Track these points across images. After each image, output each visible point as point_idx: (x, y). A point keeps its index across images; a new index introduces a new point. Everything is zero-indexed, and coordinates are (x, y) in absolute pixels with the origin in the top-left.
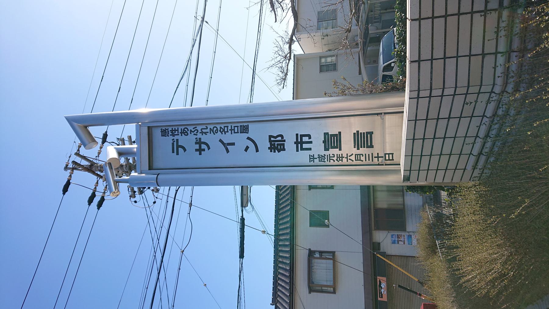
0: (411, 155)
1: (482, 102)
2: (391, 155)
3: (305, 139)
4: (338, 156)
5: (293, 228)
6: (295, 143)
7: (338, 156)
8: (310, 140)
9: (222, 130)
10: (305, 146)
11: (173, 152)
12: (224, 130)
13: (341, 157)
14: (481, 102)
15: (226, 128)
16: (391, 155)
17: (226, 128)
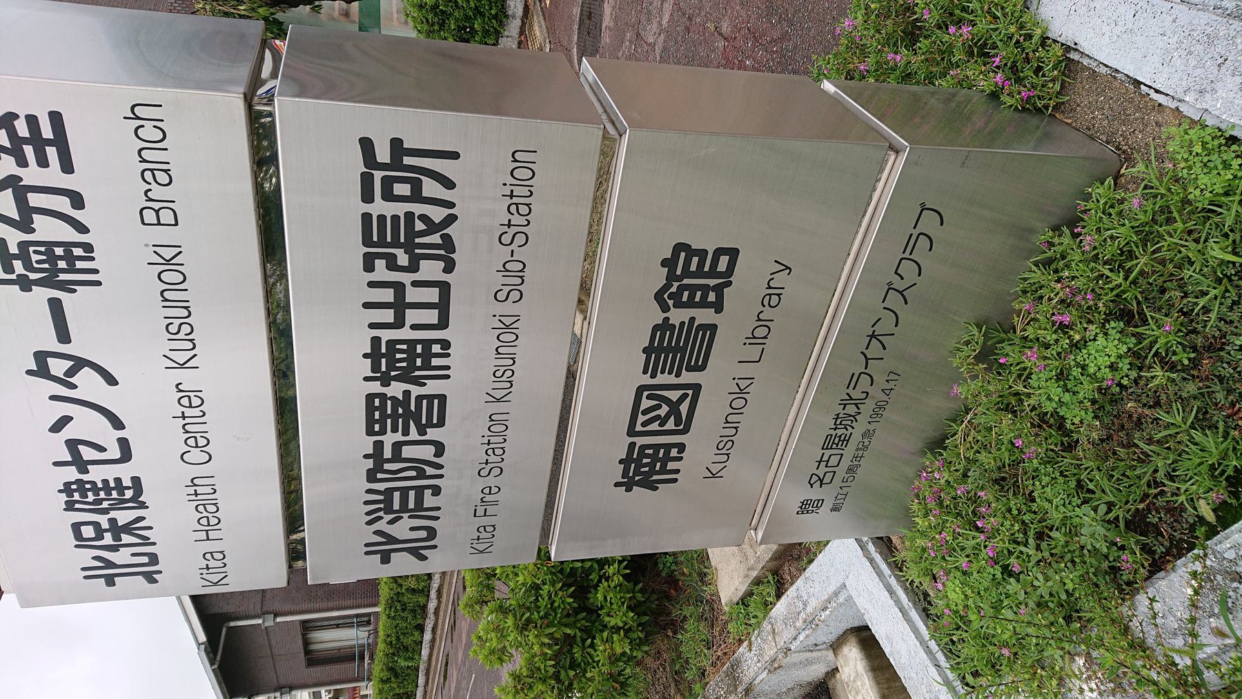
10: (388, 295)
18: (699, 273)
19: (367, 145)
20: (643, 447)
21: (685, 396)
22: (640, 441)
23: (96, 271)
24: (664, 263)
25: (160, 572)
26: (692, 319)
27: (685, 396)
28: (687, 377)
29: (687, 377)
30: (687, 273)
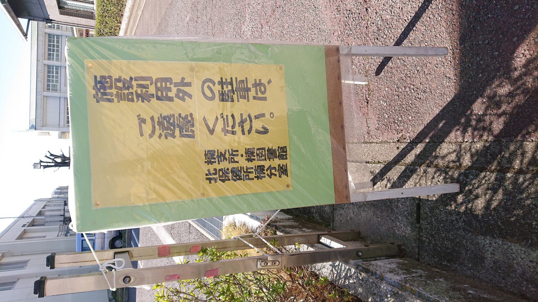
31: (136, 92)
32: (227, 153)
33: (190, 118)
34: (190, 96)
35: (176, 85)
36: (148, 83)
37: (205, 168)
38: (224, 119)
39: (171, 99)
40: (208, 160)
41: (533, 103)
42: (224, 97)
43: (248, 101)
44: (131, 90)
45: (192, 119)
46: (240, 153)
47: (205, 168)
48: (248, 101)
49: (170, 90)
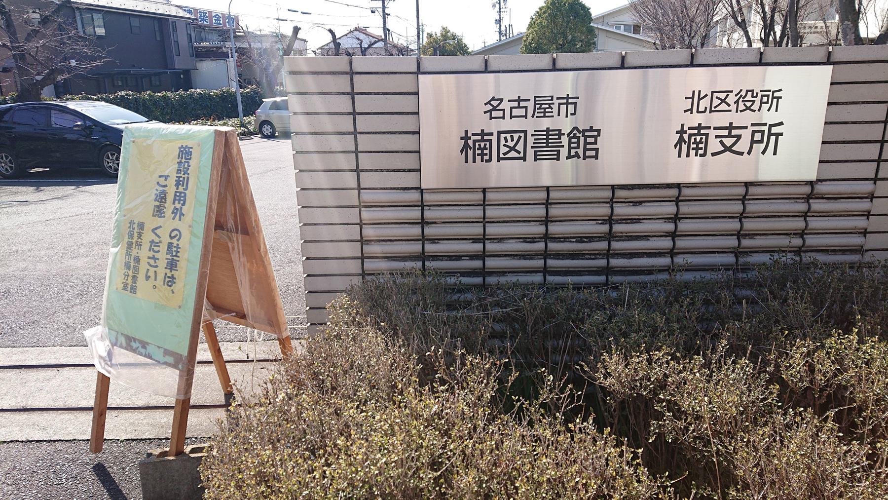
0: (91, 403)
1: (174, 291)
2: (502, 116)
3: (571, 107)
4: (542, 115)
5: (766, 13)
6: (548, 129)
7: (542, 115)
8: (569, 114)
9: (495, 103)
10: (563, 107)
11: (535, 131)
12: (495, 109)
13: (567, 101)
14: (173, 293)
15: (500, 114)
16: (502, 116)
17: (500, 114)
18: (586, 143)
19: (192, 148)
20: (490, 141)
21: (519, 153)
22: (494, 139)
23: (561, 142)
24: (591, 127)
25: (700, 92)
26: (563, 146)
27: (519, 153)
28: (530, 153)
29: (530, 153)
30: (586, 137)
31: (181, 177)
32: (141, 241)
33: (163, 215)
34: (173, 219)
35: (181, 208)
36: (185, 187)
37: (136, 221)
38: (158, 243)
39: (174, 203)
40: (686, 132)
41: (471, 412)
42: (170, 245)
43: (782, 135)
44: (182, 173)
45: (161, 217)
46: (139, 251)
47: (136, 221)
48: (782, 135)
49: (179, 203)
